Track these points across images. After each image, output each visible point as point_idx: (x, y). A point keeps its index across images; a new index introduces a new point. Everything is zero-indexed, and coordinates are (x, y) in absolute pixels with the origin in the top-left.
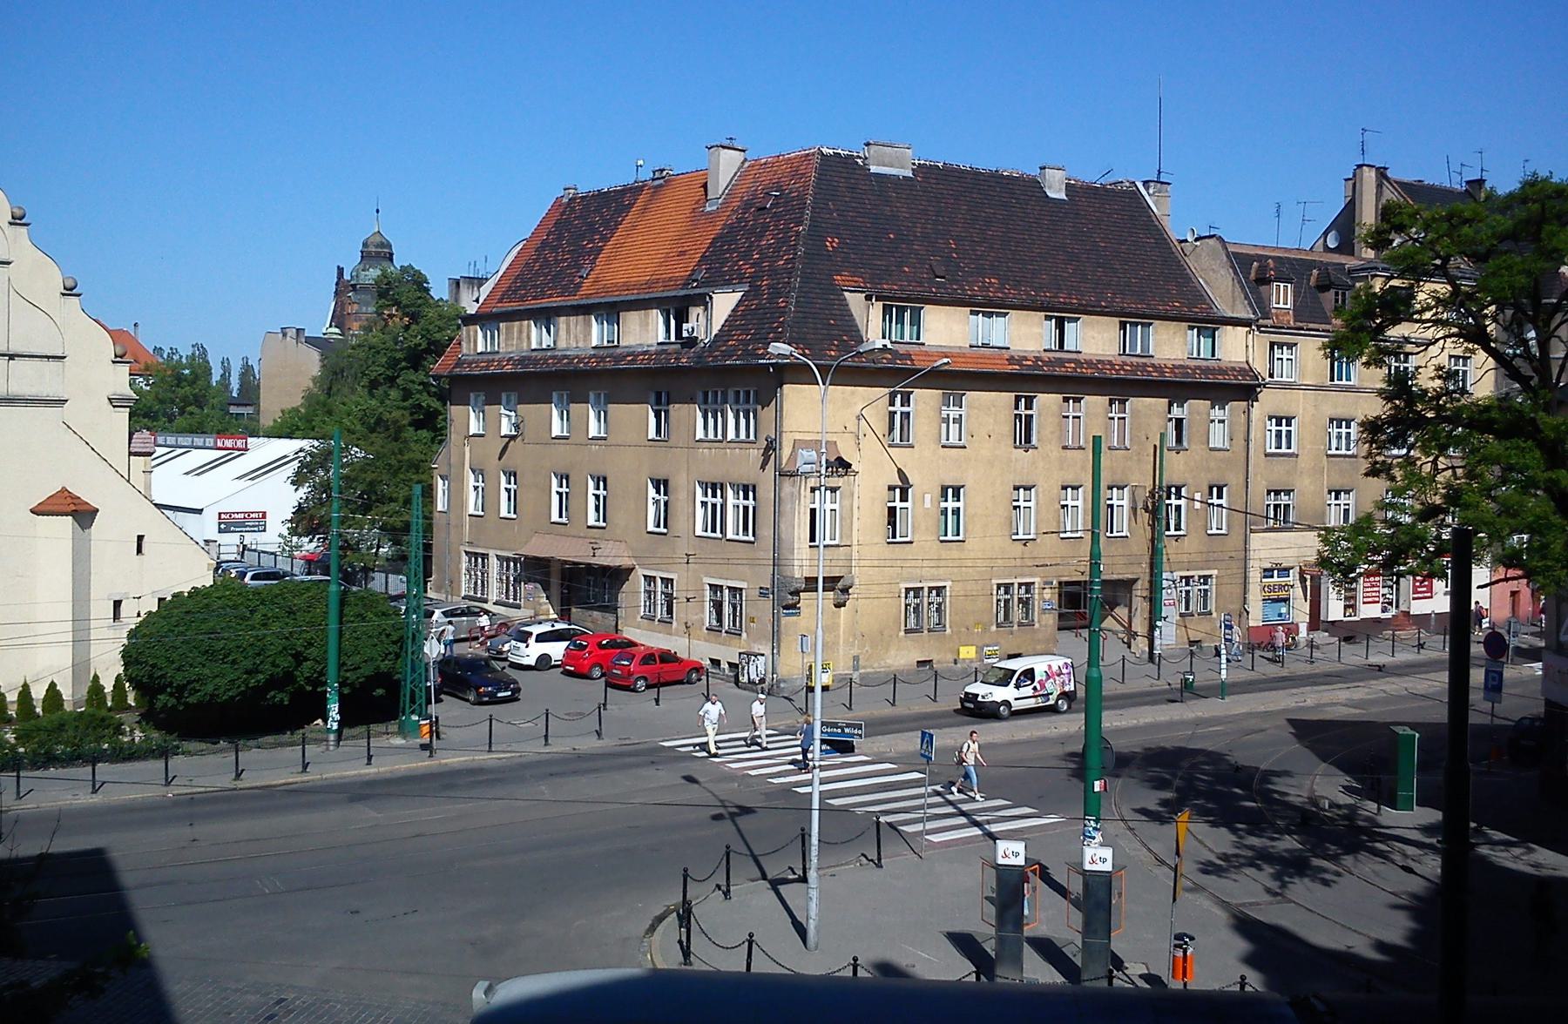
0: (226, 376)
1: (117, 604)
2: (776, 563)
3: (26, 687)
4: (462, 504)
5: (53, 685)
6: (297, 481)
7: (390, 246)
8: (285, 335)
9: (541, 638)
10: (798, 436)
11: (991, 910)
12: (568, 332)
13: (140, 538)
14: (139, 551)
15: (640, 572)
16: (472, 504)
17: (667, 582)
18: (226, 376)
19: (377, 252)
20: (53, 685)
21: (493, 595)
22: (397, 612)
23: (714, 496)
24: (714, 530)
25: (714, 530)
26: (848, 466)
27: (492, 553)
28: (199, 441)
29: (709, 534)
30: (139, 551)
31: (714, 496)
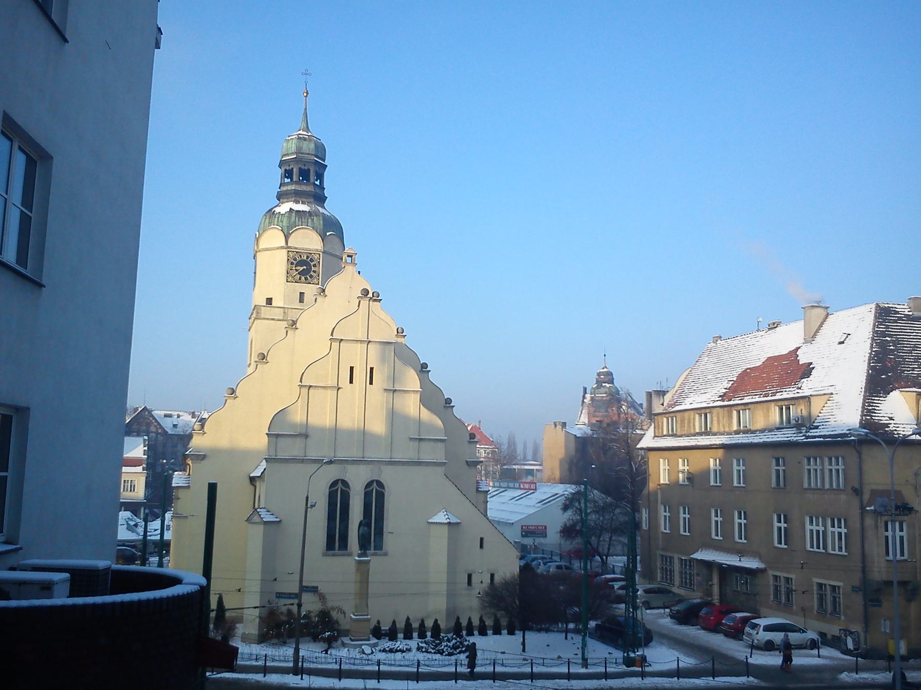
0: (525, 448)
1: (470, 576)
2: (864, 570)
3: (423, 621)
4: (657, 526)
5: (436, 621)
6: (565, 508)
7: (612, 374)
8: (556, 426)
9: (768, 628)
10: (874, 487)
11: (508, 566)
12: (719, 423)
13: (482, 539)
14: (481, 546)
15: (771, 573)
16: (664, 528)
17: (788, 580)
18: (525, 448)
19: (608, 377)
20: (436, 621)
21: (677, 583)
22: (613, 587)
23: (818, 525)
24: (818, 548)
25: (818, 548)
26: (911, 510)
27: (676, 556)
28: (511, 485)
29: (837, 552)
30: (481, 546)
31: (818, 525)
